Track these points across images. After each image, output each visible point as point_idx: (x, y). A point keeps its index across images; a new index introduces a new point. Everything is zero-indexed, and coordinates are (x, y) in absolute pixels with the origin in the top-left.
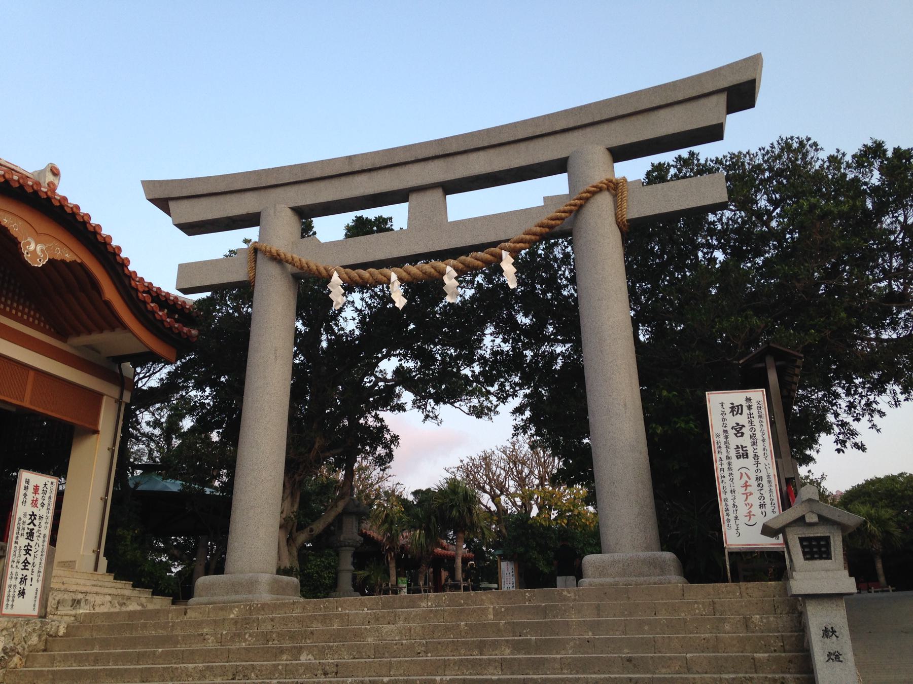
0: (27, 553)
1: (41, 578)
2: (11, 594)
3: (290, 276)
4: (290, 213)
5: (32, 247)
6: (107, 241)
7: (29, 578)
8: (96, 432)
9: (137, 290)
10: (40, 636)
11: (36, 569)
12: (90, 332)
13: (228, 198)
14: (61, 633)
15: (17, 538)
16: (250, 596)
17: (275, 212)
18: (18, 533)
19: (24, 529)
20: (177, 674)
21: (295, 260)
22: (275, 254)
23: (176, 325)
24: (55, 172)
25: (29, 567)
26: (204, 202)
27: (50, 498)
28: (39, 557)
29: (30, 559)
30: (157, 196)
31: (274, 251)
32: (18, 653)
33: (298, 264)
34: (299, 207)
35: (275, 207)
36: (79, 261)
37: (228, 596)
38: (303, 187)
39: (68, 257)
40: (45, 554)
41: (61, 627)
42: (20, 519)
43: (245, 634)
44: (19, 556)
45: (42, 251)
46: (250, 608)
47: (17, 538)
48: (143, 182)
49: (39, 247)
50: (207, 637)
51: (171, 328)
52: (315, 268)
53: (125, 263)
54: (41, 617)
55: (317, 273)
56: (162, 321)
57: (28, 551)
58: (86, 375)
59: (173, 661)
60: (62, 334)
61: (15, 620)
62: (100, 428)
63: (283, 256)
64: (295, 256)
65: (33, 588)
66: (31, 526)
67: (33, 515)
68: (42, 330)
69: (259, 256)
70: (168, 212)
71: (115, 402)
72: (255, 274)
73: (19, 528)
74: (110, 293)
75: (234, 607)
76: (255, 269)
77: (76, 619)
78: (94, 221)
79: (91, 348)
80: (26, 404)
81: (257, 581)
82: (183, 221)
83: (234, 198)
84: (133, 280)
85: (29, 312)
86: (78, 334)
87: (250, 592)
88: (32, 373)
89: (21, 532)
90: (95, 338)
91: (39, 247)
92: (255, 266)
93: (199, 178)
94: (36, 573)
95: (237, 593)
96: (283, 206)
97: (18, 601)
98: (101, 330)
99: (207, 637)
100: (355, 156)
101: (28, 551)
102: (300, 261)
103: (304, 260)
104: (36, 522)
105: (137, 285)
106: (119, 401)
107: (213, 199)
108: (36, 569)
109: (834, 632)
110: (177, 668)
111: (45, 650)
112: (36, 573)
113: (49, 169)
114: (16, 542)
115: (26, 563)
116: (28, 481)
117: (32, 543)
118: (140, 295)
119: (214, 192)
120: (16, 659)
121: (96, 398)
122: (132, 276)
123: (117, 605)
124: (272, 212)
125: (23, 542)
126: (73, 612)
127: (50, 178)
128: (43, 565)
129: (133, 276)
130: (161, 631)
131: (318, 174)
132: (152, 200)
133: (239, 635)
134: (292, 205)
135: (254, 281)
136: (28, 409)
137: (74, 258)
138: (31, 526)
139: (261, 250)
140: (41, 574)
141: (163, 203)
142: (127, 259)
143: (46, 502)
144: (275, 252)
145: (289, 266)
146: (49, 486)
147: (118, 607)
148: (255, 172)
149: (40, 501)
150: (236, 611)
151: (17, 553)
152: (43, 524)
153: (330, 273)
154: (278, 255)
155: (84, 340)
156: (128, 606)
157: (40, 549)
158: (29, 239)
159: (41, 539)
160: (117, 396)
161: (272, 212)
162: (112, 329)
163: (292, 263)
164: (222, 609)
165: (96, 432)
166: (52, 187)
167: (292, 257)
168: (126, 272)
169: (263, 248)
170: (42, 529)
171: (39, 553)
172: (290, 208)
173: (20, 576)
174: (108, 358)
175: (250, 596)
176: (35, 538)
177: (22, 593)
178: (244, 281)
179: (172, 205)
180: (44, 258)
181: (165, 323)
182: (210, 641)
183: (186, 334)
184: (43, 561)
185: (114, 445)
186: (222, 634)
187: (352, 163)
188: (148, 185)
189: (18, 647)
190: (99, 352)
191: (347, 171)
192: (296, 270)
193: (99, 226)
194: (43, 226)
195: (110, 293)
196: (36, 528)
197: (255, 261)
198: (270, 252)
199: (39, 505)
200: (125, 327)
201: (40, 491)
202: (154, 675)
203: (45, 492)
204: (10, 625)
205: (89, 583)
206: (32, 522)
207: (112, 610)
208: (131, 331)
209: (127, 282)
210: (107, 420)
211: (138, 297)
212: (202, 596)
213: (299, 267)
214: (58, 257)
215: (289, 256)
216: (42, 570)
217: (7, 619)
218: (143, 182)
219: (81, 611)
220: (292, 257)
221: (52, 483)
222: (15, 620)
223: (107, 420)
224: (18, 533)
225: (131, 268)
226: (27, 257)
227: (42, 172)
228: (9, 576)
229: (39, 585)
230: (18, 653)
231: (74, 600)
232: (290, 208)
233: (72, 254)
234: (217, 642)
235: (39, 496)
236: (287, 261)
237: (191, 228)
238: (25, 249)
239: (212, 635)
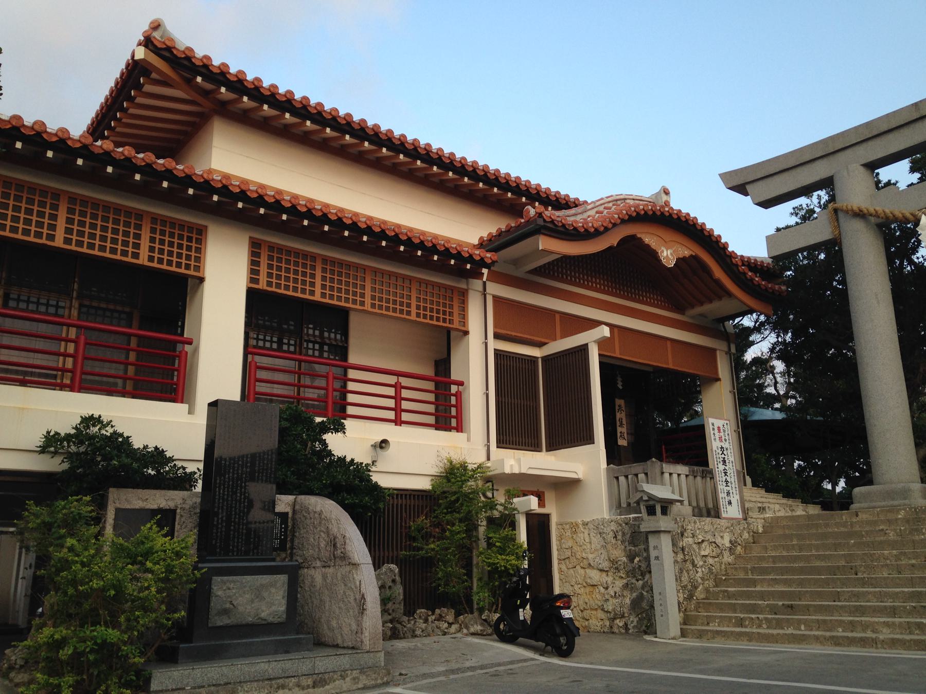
0: (726, 475)
1: (738, 492)
2: (724, 503)
3: (875, 227)
4: (862, 169)
5: (665, 254)
6: (710, 233)
7: (731, 492)
8: (718, 380)
9: (737, 265)
10: (749, 533)
11: (733, 485)
12: (702, 304)
13: (799, 170)
14: (760, 531)
15: (717, 464)
16: (907, 502)
17: (848, 173)
18: (717, 461)
19: (719, 458)
20: (875, 558)
21: (879, 212)
22: (858, 211)
23: (763, 283)
24: (667, 192)
25: (729, 484)
26: (777, 178)
27: (728, 434)
28: (733, 477)
29: (728, 479)
30: (735, 184)
31: (855, 208)
32: (739, 544)
33: (882, 215)
34: (871, 162)
35: (847, 168)
36: (694, 254)
37: (886, 502)
38: (870, 143)
39: (687, 253)
40: (735, 474)
41: (759, 527)
42: (715, 451)
43: (922, 529)
44: (722, 477)
45: (671, 254)
46: (915, 510)
47: (717, 464)
48: (720, 175)
49: (669, 252)
50: (887, 532)
51: (766, 290)
52: (900, 215)
53: (725, 246)
54: (744, 520)
55: (904, 219)
56: (759, 285)
57: (726, 473)
58: (701, 336)
59: (866, 549)
60: (680, 309)
61: (732, 522)
62: (721, 376)
63: (866, 211)
64: (877, 208)
65: (735, 498)
66: (723, 456)
67: (722, 448)
68: (603, 292)
69: (841, 215)
70: (746, 194)
71: (726, 354)
72: (840, 231)
73: (716, 457)
74: (718, 273)
75: (901, 510)
76: (839, 227)
77: (765, 521)
78: (700, 221)
79: (701, 315)
80: (671, 366)
81: (910, 490)
82: (762, 199)
83: (806, 169)
84: (733, 258)
85: (579, 276)
86: (693, 307)
87: (905, 499)
88: (669, 343)
89: (718, 460)
90: (707, 308)
91: (669, 252)
92: (838, 224)
93: (769, 160)
94: (734, 489)
95: (893, 499)
96: (855, 165)
97: (729, 508)
98: (711, 301)
99: (887, 532)
100: (921, 101)
101: (726, 473)
102: (884, 212)
103: (887, 211)
104: (725, 452)
105: (736, 261)
106: (728, 352)
107: (786, 175)
108: (733, 485)
109: (381, 447)
110: (874, 554)
111: (754, 543)
112: (734, 489)
113: (663, 191)
114: (718, 468)
115: (727, 481)
116: (713, 424)
117: (727, 468)
118: (740, 268)
119: (785, 168)
120: (739, 548)
121: (712, 352)
122: (732, 255)
123: (789, 511)
124: (845, 173)
125: (721, 467)
126: (762, 516)
127: (665, 198)
128: (736, 482)
129: (733, 255)
130: (842, 528)
131: (885, 127)
132: (730, 188)
133: (917, 530)
134: (863, 163)
135: (841, 238)
136: (673, 369)
137: (691, 253)
138: (723, 456)
139: (842, 210)
140: (737, 489)
141: (741, 189)
142: (726, 243)
143: (727, 438)
144: (857, 209)
145: (872, 219)
146: (725, 426)
147: (790, 512)
148: (821, 141)
149: (723, 438)
150: (902, 513)
151: (720, 475)
152: (729, 454)
153: (918, 217)
154: (861, 211)
155: (699, 310)
156: (796, 512)
157: (732, 471)
158: (663, 248)
159: (731, 464)
160: (726, 349)
161: (845, 173)
162: (720, 298)
163: (877, 215)
164: (889, 511)
165: (718, 380)
166: (667, 203)
167: (875, 210)
168: (728, 253)
169: (845, 208)
170: (730, 457)
171: (732, 474)
172: (862, 165)
173: (726, 491)
174: (713, 320)
175: (907, 502)
176: (727, 464)
177: (730, 503)
178: (830, 240)
179: (748, 188)
180: (674, 259)
181: (762, 286)
182: (891, 535)
183: (778, 291)
184: (736, 480)
185: (734, 389)
186: (900, 530)
187: (919, 109)
188: (725, 177)
189: (738, 540)
190: (706, 317)
191: (915, 118)
192: (880, 221)
193: (704, 224)
194: (669, 235)
195: (718, 273)
196: (726, 457)
197: (837, 220)
198: (852, 210)
199: (723, 441)
200: (729, 294)
201: (722, 431)
202: (856, 558)
203: (724, 431)
204: (730, 525)
205: (758, 496)
206: (723, 453)
207: (787, 515)
208: (736, 298)
209: (729, 261)
210: (723, 369)
211: (739, 270)
212: (861, 503)
213: (884, 217)
214: (681, 256)
215: (872, 210)
216: (737, 486)
217: (727, 521)
218: (720, 175)
219: (768, 516)
220: (875, 210)
221: (727, 424)
222: (732, 522)
223: (723, 369)
224: (717, 461)
225: (730, 249)
226: (664, 261)
227: (658, 194)
228: (720, 491)
229: (737, 497)
230: (739, 544)
231: (760, 508)
232: (862, 165)
233: (689, 251)
234: (897, 535)
235: (722, 434)
236: (871, 215)
237: (766, 204)
238: (662, 256)
239: (892, 530)
